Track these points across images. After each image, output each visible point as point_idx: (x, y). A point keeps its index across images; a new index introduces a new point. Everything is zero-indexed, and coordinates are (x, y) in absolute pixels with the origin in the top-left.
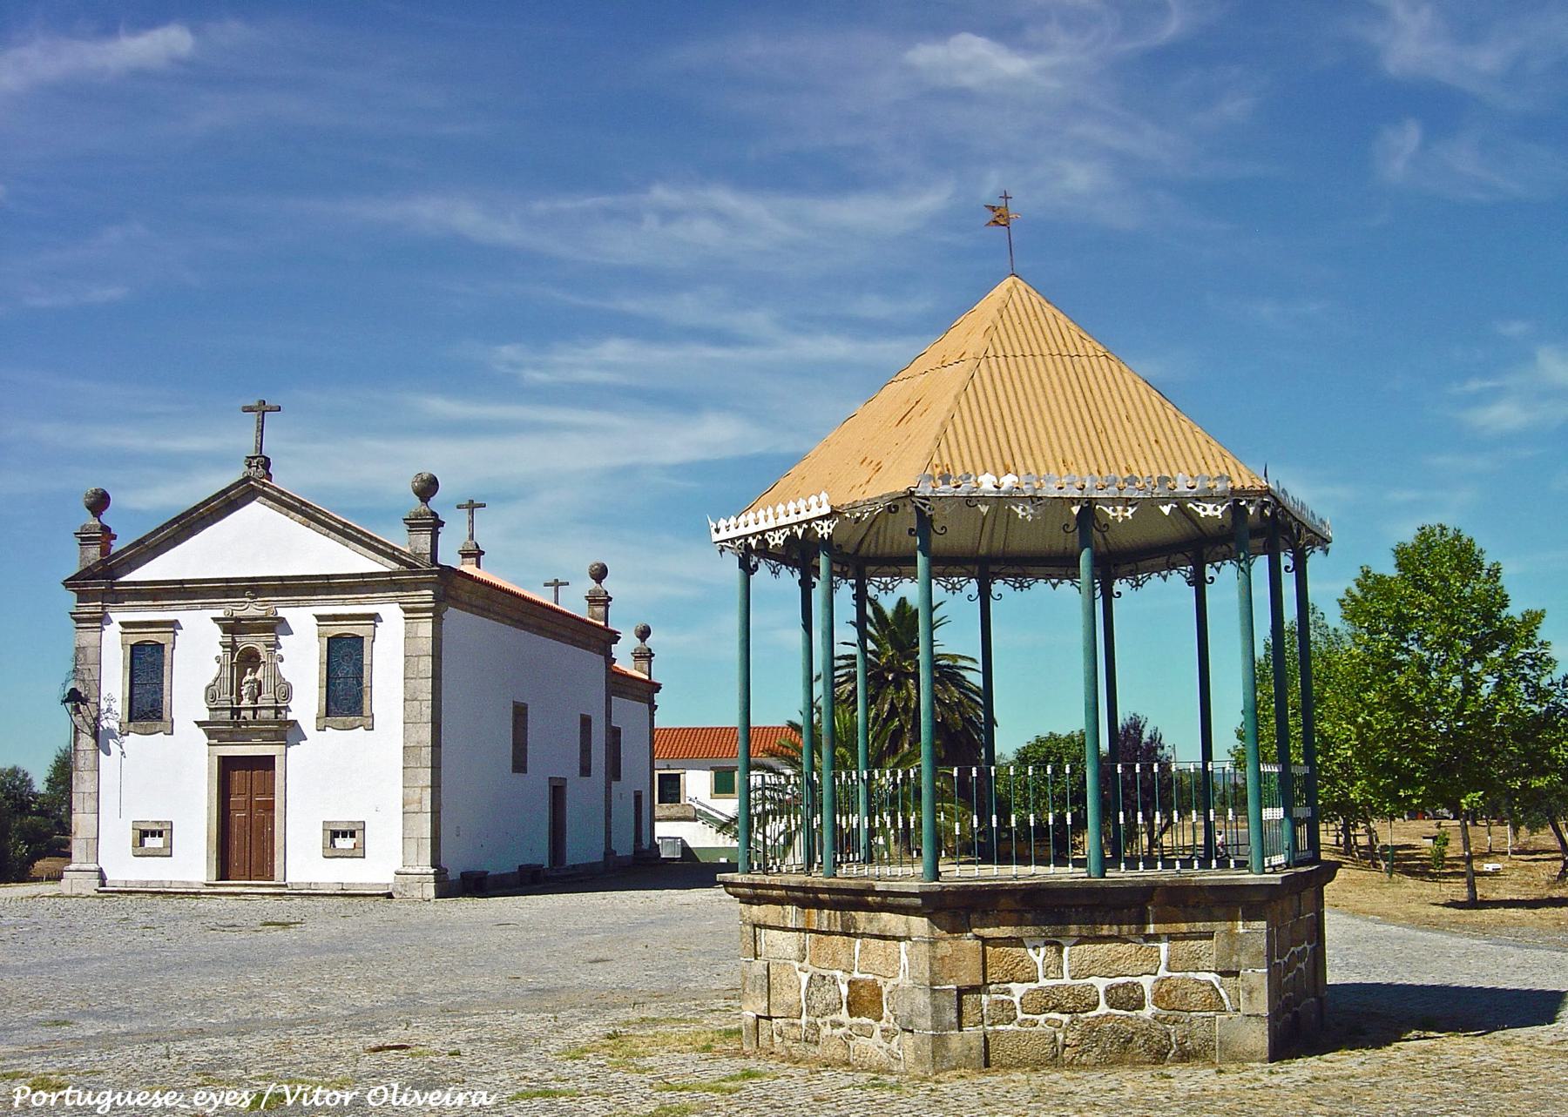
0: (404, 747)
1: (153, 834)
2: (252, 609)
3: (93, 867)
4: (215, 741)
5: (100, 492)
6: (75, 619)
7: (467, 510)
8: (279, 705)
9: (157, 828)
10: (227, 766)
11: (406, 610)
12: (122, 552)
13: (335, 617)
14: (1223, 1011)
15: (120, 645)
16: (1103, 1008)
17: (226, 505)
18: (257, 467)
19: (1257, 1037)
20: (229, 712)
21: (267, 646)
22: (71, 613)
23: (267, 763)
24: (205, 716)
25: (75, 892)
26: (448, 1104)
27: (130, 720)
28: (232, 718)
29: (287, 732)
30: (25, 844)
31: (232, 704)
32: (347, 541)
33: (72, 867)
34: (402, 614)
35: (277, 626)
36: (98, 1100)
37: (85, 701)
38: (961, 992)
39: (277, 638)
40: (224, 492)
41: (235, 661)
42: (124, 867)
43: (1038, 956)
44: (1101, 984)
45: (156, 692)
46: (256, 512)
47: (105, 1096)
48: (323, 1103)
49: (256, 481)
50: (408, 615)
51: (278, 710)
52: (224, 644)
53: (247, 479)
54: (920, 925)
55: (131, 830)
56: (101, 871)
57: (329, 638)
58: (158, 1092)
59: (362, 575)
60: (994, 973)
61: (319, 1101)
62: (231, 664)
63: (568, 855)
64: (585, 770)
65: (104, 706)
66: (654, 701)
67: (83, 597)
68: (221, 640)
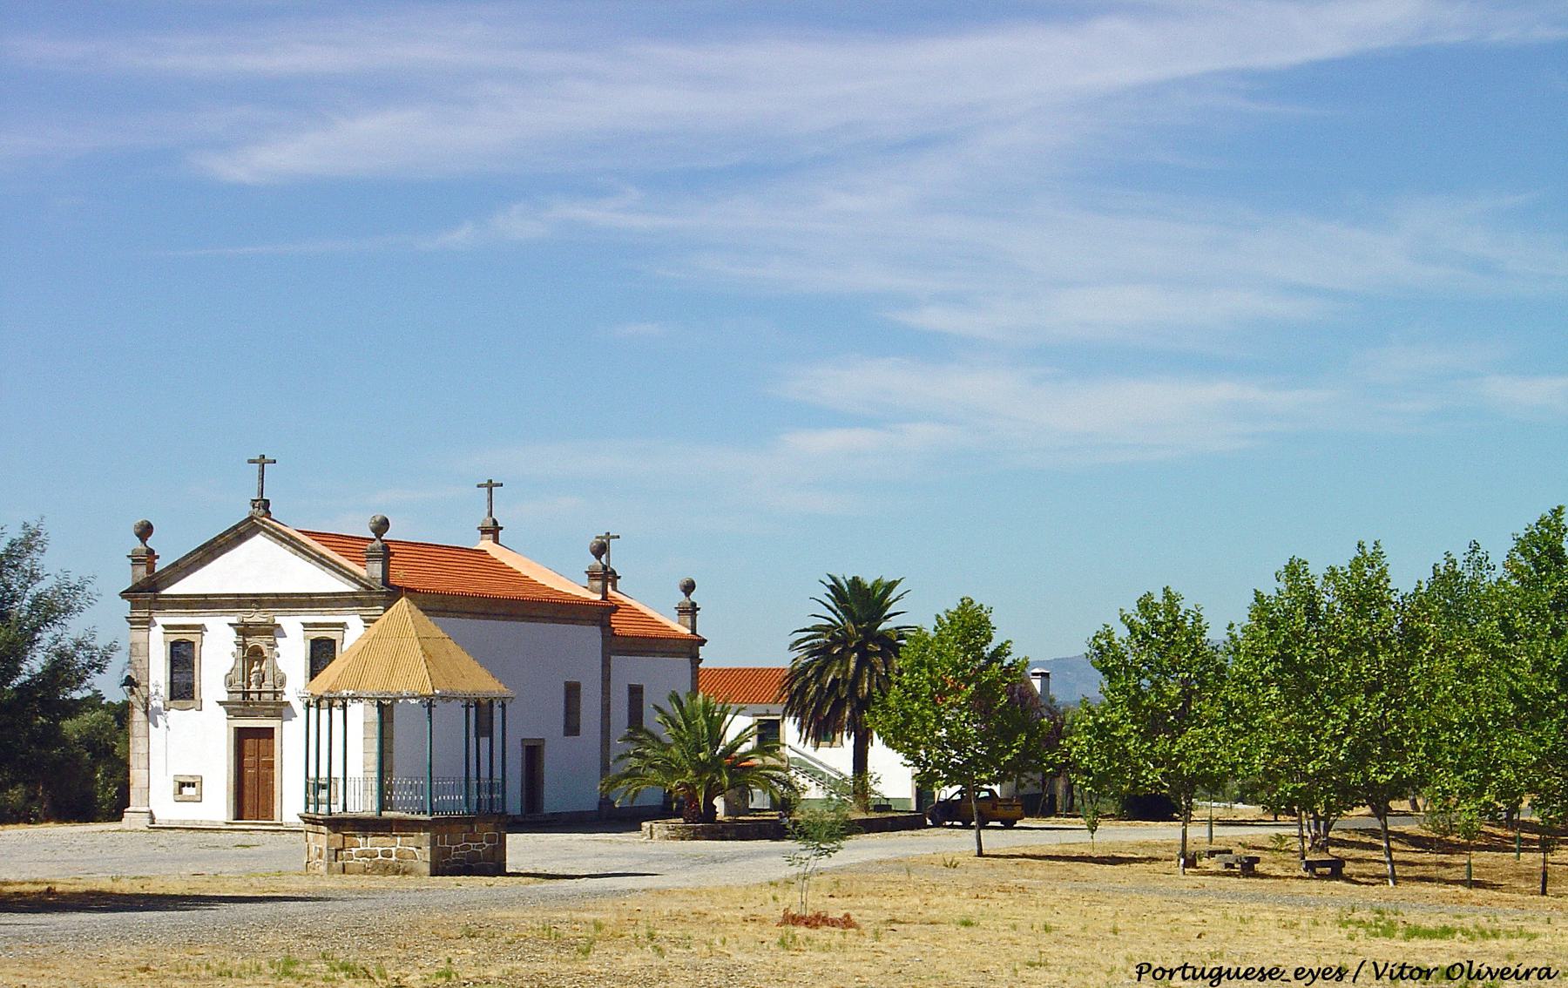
0: (364, 723)
1: (189, 785)
2: (257, 617)
3: (146, 809)
4: (232, 716)
5: (145, 523)
6: (130, 622)
7: (486, 489)
9: (191, 780)
10: (241, 735)
11: (365, 621)
12: (162, 571)
13: (316, 625)
14: (416, 859)
15: (163, 643)
16: (380, 857)
17: (237, 537)
18: (259, 509)
19: (426, 868)
20: (241, 695)
21: (268, 645)
22: (127, 618)
23: (268, 733)
24: (225, 698)
25: (132, 828)
27: (171, 699)
28: (244, 699)
29: (281, 710)
30: (115, 786)
32: (323, 567)
33: (129, 809)
34: (362, 623)
35: (273, 630)
37: (137, 685)
38: (337, 850)
39: (275, 640)
40: (235, 527)
41: (245, 655)
42: (167, 809)
43: (361, 840)
44: (379, 849)
45: (189, 679)
46: (259, 544)
49: (257, 519)
50: (367, 625)
51: (276, 694)
53: (251, 518)
54: (324, 829)
55: (173, 782)
56: (151, 812)
57: (312, 640)
59: (334, 594)
60: (347, 845)
63: (546, 802)
64: (572, 728)
65: (152, 690)
66: (698, 655)
67: (135, 606)
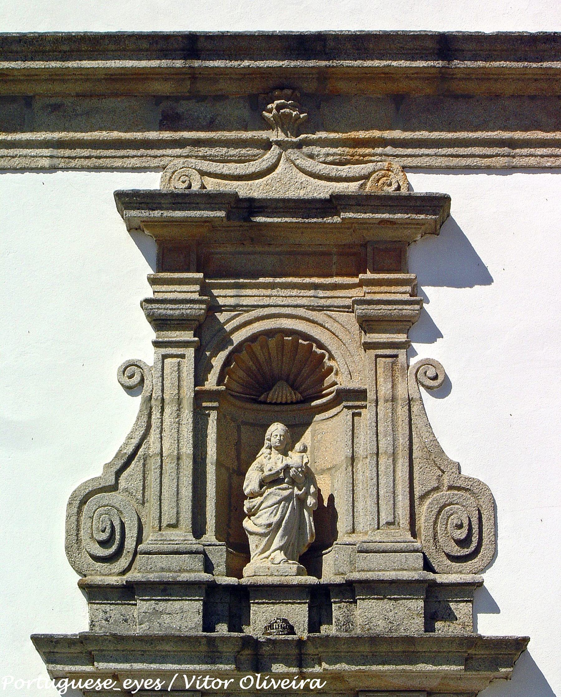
8: (441, 578)
26: (294, 687)
28: (208, 626)
31: (208, 567)
41: (211, 383)
47: (64, 682)
48: (210, 686)
52: (162, 310)
58: (99, 680)
62: (199, 397)
68: (150, 294)
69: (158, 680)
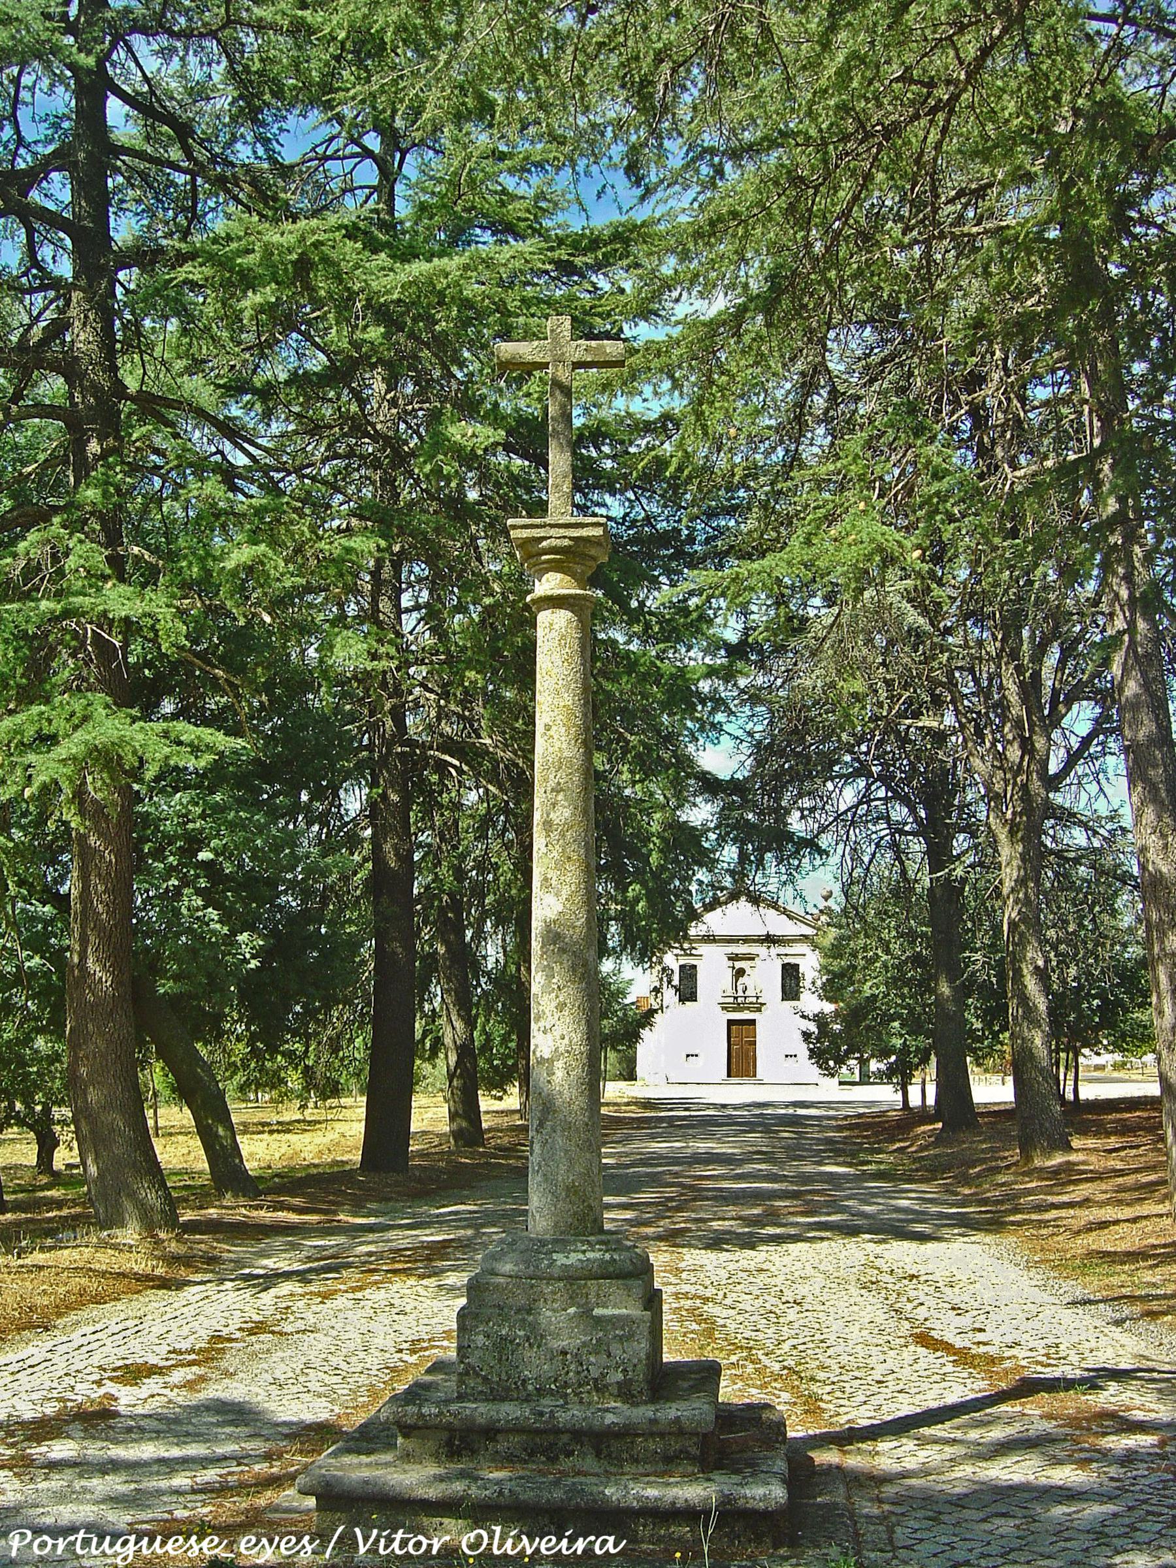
23: (753, 1022)
26: (564, 1552)
36: (118, 1547)
61: (401, 1548)
69: (307, 1538)
